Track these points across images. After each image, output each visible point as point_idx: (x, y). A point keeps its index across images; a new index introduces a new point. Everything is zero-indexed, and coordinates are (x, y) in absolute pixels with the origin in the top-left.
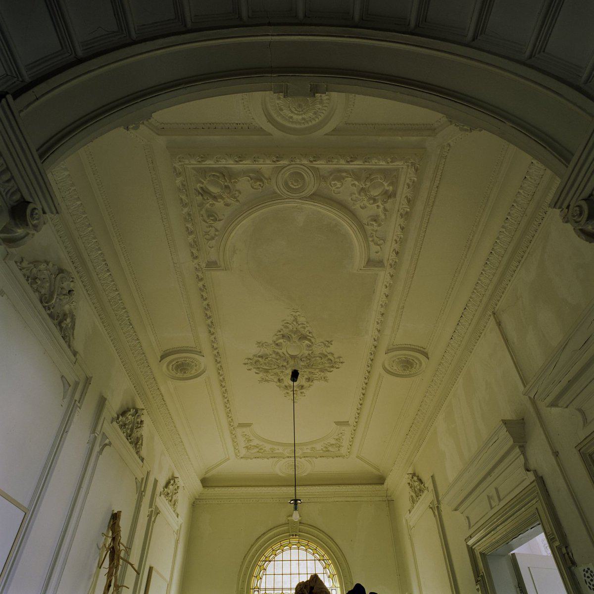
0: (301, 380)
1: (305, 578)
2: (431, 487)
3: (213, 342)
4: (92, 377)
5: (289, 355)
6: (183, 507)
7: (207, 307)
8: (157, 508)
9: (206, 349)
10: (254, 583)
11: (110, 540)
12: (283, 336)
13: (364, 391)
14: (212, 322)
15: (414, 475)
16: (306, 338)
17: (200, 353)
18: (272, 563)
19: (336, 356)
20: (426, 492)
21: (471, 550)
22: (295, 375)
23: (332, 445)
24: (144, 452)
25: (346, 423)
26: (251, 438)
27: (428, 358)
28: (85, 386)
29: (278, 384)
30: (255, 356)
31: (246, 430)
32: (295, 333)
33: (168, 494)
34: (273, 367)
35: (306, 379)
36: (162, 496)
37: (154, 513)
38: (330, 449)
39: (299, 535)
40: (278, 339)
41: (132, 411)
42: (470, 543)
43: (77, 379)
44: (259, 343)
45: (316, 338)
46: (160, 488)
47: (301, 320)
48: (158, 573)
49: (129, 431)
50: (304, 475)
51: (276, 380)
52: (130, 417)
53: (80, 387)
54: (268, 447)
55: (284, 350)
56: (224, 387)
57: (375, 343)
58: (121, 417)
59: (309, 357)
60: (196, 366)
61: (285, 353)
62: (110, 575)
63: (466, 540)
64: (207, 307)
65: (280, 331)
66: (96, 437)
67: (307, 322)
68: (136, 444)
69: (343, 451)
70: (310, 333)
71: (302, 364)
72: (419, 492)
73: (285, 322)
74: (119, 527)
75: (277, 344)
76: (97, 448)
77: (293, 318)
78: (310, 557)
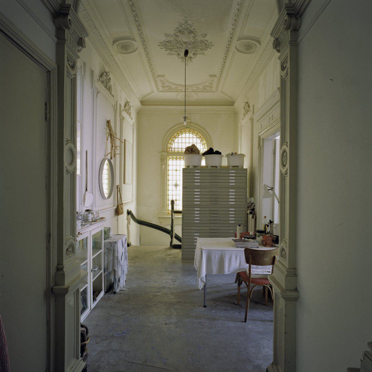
0: (190, 55)
1: (190, 145)
2: (252, 110)
3: (141, 35)
4: (86, 62)
5: (183, 41)
6: (133, 115)
7: (132, 5)
8: (123, 117)
9: (137, 38)
10: (169, 146)
11: (108, 131)
12: (179, 31)
13: (224, 61)
14: (139, 24)
15: (247, 103)
16: (192, 32)
17: (134, 39)
18: (177, 138)
19: (209, 42)
20: (250, 112)
21: (259, 137)
22: (186, 53)
23: (207, 86)
24: (113, 93)
25: (215, 76)
26: (165, 82)
27: (260, 44)
28: (84, 67)
29: (178, 56)
30: (164, 41)
31: (162, 79)
32: (186, 30)
33: (103, 81)
34: (175, 47)
35: (193, 54)
36: (124, 111)
37: (122, 119)
38: (207, 88)
39: (190, 128)
40: (177, 33)
41: (105, 74)
42: (260, 135)
43: (81, 65)
44: (166, 34)
45: (198, 32)
46: (122, 108)
47: (189, 22)
48: (127, 141)
49: (105, 84)
50: (193, 100)
51: (176, 54)
52: (104, 77)
53: (83, 66)
54: (174, 87)
55: (180, 39)
56: (149, 58)
57: (231, 36)
58: (101, 78)
59: (194, 43)
60: (132, 46)
61: (181, 40)
62: (112, 143)
63: (259, 134)
64: (132, 5)
65: (177, 29)
66: (94, 90)
67: (193, 24)
68: (109, 89)
69: (214, 89)
70: (194, 30)
71: (190, 46)
72: (247, 111)
73: (180, 23)
74: (111, 126)
75: (176, 35)
76: (95, 95)
77: (184, 21)
78: (194, 136)
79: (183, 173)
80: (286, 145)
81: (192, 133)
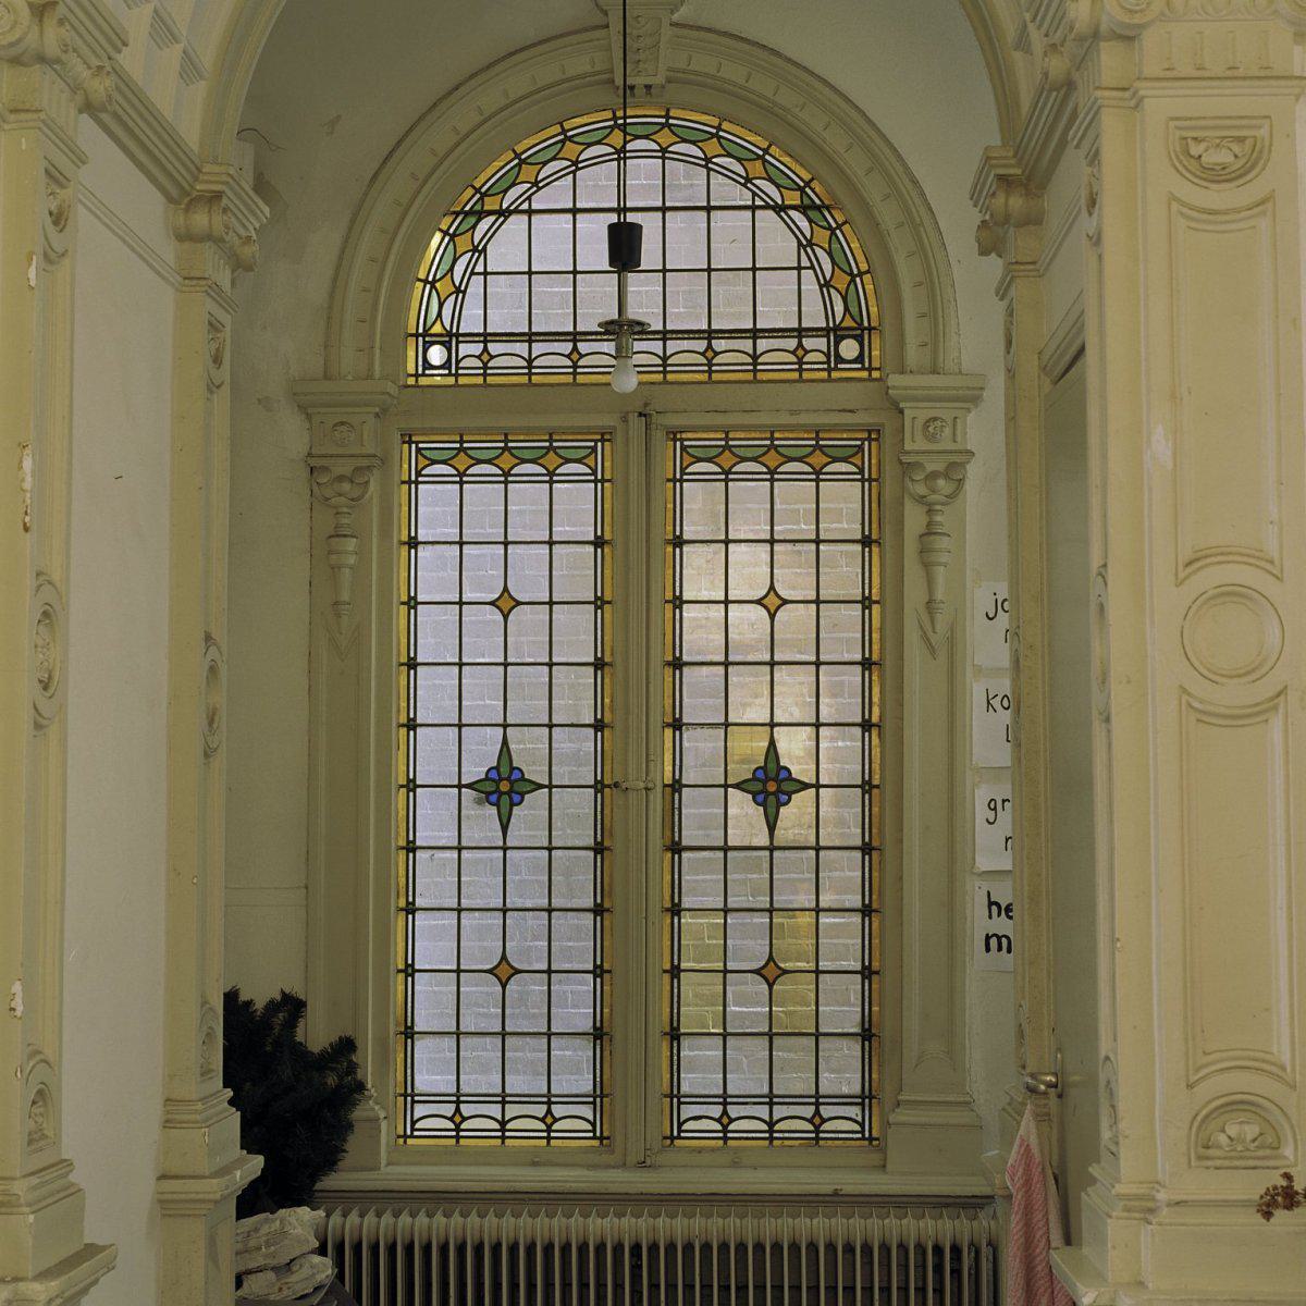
18: (517, 223)
78: (728, 191)
79: (225, 998)
80: (40, 714)
81: (695, 151)
